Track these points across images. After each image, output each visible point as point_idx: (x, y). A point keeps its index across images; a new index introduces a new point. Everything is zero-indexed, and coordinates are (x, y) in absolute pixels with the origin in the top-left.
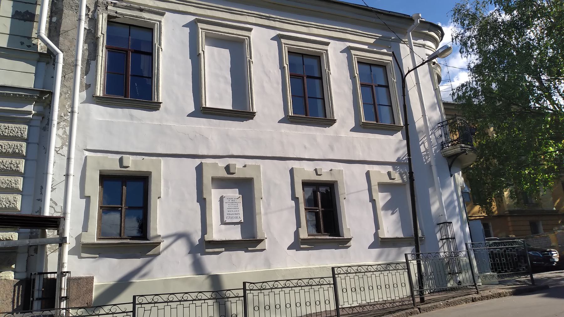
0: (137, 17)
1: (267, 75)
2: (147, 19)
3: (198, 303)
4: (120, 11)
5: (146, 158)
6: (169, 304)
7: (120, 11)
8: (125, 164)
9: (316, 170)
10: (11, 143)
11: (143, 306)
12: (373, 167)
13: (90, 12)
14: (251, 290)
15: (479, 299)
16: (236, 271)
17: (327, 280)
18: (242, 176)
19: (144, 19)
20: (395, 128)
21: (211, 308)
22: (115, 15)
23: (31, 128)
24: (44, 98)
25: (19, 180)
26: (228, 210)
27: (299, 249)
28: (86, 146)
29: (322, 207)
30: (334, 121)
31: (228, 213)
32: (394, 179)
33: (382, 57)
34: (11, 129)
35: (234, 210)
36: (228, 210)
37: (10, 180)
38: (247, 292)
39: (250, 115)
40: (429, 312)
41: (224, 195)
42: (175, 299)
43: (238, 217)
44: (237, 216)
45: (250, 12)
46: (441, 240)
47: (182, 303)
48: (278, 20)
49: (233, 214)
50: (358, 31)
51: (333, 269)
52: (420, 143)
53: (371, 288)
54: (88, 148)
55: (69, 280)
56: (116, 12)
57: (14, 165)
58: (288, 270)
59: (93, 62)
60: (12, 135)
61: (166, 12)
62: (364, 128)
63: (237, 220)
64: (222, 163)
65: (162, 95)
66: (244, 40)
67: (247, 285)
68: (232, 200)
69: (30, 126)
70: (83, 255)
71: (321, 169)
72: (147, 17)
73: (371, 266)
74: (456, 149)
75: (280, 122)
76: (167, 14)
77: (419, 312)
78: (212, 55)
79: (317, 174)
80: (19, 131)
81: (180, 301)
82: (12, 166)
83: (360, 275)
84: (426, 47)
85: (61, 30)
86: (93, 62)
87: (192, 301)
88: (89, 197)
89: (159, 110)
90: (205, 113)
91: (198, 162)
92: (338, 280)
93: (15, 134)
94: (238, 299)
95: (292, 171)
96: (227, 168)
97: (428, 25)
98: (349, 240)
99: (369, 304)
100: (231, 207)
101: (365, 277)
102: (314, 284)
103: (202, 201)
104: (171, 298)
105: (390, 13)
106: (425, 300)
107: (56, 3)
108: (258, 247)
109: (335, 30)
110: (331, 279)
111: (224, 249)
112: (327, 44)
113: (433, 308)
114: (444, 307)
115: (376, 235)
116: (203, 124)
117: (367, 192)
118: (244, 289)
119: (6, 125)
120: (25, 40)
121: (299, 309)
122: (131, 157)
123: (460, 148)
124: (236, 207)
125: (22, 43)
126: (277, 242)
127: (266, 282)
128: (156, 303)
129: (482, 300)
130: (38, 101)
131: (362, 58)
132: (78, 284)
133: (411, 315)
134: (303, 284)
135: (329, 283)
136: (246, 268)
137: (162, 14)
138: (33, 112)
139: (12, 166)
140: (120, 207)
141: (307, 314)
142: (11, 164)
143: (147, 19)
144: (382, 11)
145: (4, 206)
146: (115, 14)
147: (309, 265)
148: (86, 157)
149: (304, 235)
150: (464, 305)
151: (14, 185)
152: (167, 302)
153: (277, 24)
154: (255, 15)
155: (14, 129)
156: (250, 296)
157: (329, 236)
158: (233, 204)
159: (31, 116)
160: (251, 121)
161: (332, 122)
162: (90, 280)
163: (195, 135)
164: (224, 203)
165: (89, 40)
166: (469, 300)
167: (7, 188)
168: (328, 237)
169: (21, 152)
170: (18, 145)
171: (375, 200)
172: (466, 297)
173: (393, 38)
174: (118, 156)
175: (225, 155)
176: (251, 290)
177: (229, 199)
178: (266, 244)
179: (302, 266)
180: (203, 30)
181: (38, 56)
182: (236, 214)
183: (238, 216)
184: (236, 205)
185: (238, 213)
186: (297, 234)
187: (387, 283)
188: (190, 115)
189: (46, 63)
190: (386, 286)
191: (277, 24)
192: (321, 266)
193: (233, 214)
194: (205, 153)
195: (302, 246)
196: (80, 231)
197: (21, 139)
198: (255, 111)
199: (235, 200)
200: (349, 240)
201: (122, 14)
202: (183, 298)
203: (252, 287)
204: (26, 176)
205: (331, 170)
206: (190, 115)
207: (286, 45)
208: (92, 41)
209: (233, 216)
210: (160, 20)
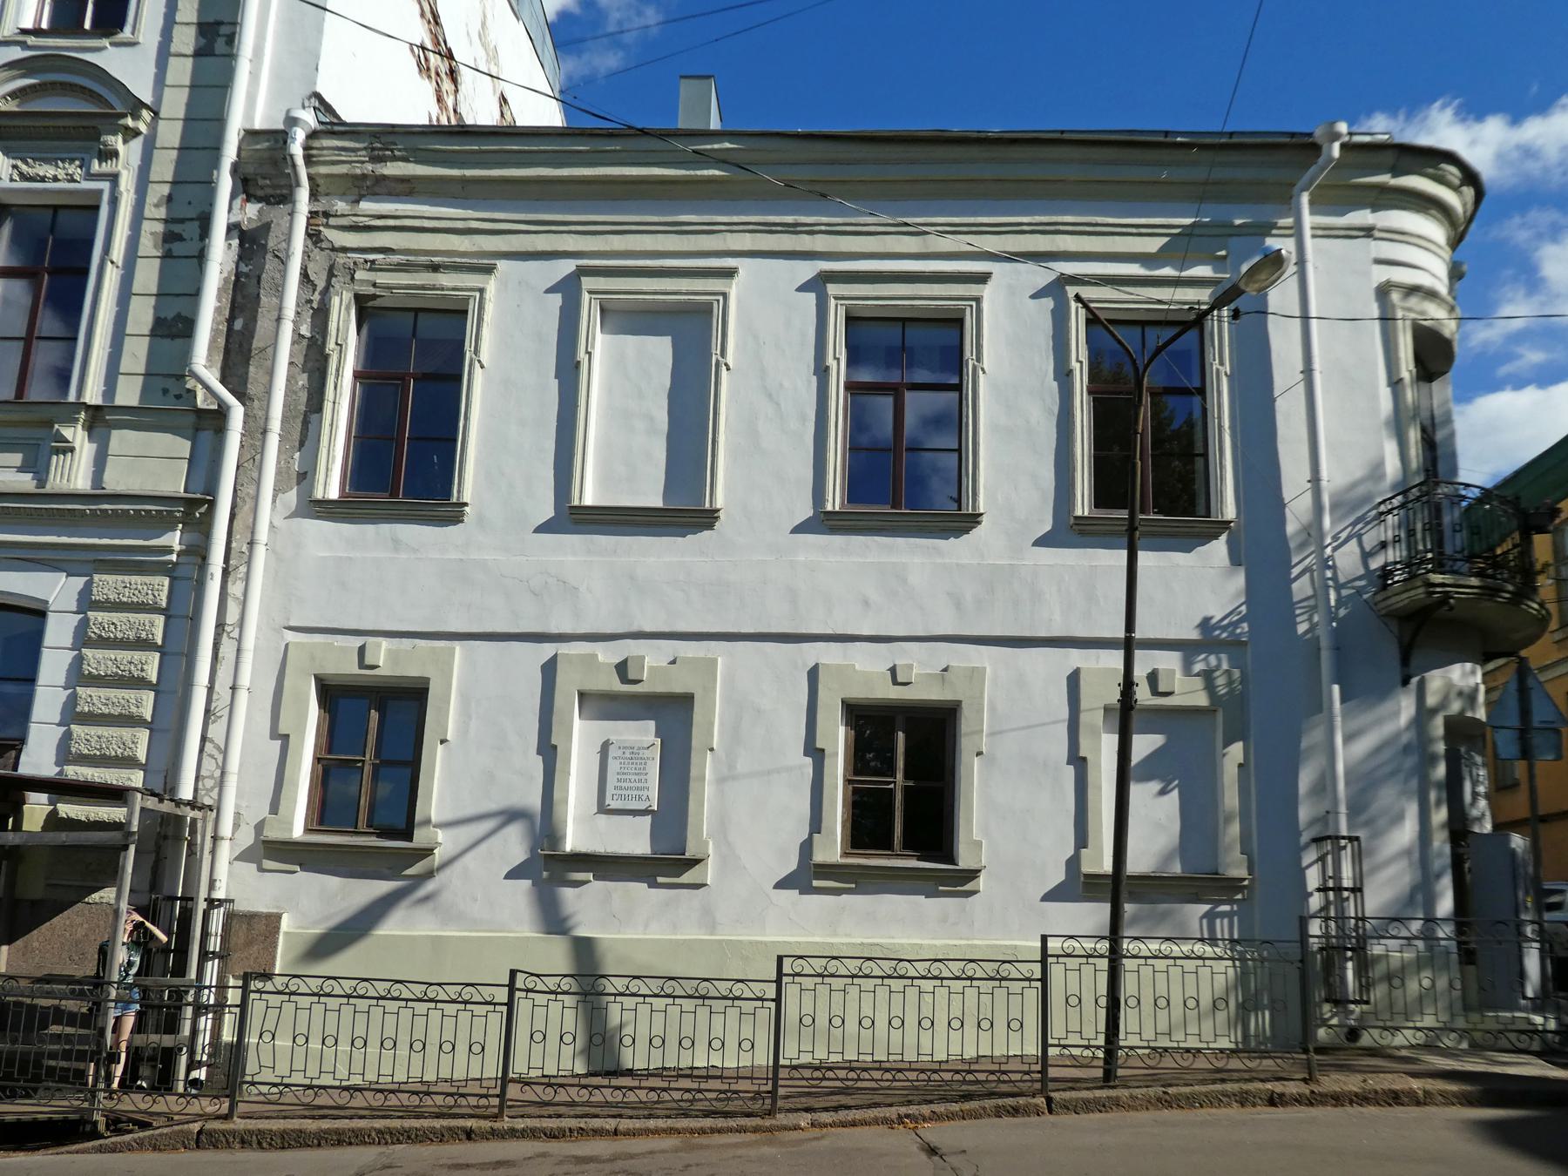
0: (423, 287)
1: (770, 396)
2: (448, 289)
3: (392, 1006)
4: (383, 278)
5: (417, 642)
6: (323, 999)
7: (383, 278)
8: (369, 661)
9: (893, 670)
10: (132, 617)
11: (264, 996)
12: (1098, 657)
13: (317, 293)
14: (528, 990)
15: (1296, 1100)
16: (619, 932)
18: (660, 688)
19: (443, 289)
20: (1197, 530)
21: (570, 1015)
22: (371, 290)
23: (176, 582)
24: (198, 515)
25: (144, 697)
26: (619, 777)
27: (807, 890)
28: (289, 620)
29: (907, 776)
30: (974, 520)
31: (619, 784)
33: (1185, 295)
34: (135, 586)
35: (633, 777)
36: (619, 777)
37: (127, 697)
38: (518, 994)
39: (705, 519)
40: (1083, 1116)
41: (613, 738)
42: (338, 991)
43: (644, 798)
44: (641, 793)
45: (735, 219)
46: (1319, 890)
47: (352, 1001)
48: (823, 228)
49: (631, 788)
50: (1100, 220)
52: (1295, 572)
54: (293, 623)
55: (230, 917)
56: (374, 285)
57: (136, 665)
58: (761, 942)
59: (314, 417)
60: (135, 600)
61: (497, 262)
62: (1082, 533)
63: (642, 806)
64: (607, 654)
65: (470, 483)
66: (710, 304)
67: (520, 977)
68: (633, 752)
69: (173, 579)
70: (268, 864)
71: (910, 667)
72: (450, 284)
73: (909, 961)
74: (1412, 593)
75: (800, 529)
76: (502, 265)
77: (1046, 1111)
78: (617, 363)
79: (895, 682)
80: (150, 592)
81: (349, 996)
82: (132, 668)
84: (1377, 234)
85: (254, 346)
86: (314, 417)
87: (378, 999)
88: (288, 736)
89: (462, 521)
90: (577, 522)
91: (547, 650)
93: (142, 599)
94: (491, 1008)
95: (813, 674)
96: (622, 668)
97: (1389, 157)
98: (972, 874)
99: (879, 1066)
100: (626, 771)
102: (713, 993)
103: (549, 751)
104: (833, 966)
105: (1235, 140)
107: (244, 283)
108: (686, 878)
111: (590, 876)
112: (983, 278)
113: (1104, 1106)
114: (1147, 1109)
115: (1073, 863)
116: (573, 548)
117: (1063, 730)
118: (511, 987)
119: (127, 578)
120: (170, 384)
121: (926, 1038)
122: (385, 643)
123: (1421, 590)
124: (640, 769)
125: (165, 391)
126: (745, 868)
127: (334, 978)
128: (798, 975)
129: (1312, 1104)
130: (188, 522)
132: (250, 928)
133: (1014, 1116)
135: (760, 995)
136: (646, 926)
137: (489, 270)
138: (177, 547)
139: (132, 668)
140: (359, 761)
141: (455, 1077)
142: (130, 663)
143: (448, 289)
144: (1259, 140)
145: (113, 754)
146: (371, 288)
147: (835, 934)
148: (287, 645)
150: (1234, 1112)
151: (134, 709)
152: (320, 996)
153: (820, 243)
154: (751, 227)
155: (139, 587)
156: (523, 1006)
157: (918, 860)
158: (632, 763)
159: (174, 557)
160: (707, 533)
161: (965, 522)
162: (273, 921)
163: (546, 583)
164: (610, 760)
165: (310, 365)
166: (1254, 1097)
167: (121, 715)
168: (913, 863)
169: (150, 636)
170: (147, 623)
171: (1084, 759)
172: (1246, 1087)
173: (1238, 222)
174: (357, 642)
175: (620, 631)
176: (528, 990)
177: (624, 748)
178: (710, 872)
179: (813, 935)
180: (593, 296)
181: (191, 418)
182: (638, 789)
183: (645, 793)
184: (641, 764)
185: (645, 785)
186: (806, 848)
188: (543, 529)
189: (211, 432)
190: (840, 1023)
191: (820, 243)
192: (865, 941)
193: (631, 788)
194: (567, 628)
195: (816, 883)
196: (264, 811)
197: (153, 609)
198: (718, 506)
199: (641, 752)
200: (972, 874)
201: (389, 288)
202: (355, 990)
203: (799, 966)
204: (161, 688)
205: (945, 670)
206: (543, 529)
207: (843, 302)
208: (317, 365)
209: (629, 792)
210: (481, 286)
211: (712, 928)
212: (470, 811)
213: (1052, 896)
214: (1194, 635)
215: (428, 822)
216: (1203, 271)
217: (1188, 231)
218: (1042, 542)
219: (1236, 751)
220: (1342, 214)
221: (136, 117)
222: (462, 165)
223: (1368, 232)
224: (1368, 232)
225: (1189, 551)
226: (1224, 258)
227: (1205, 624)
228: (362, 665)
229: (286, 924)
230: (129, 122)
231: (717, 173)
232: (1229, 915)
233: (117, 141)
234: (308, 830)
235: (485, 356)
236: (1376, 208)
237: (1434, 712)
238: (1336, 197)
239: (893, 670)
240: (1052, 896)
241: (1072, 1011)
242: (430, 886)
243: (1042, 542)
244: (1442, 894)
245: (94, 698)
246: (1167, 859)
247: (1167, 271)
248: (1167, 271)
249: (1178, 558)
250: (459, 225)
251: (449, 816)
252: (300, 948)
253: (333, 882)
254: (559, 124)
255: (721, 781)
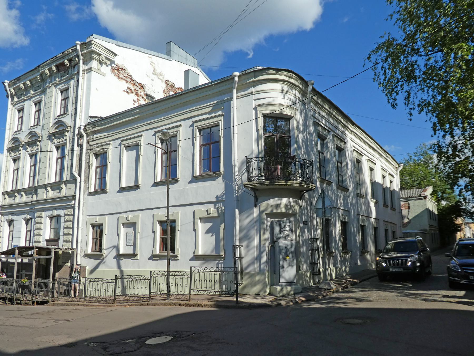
9: (207, 211)
17: (113, 280)
18: (132, 222)
32: (210, 214)
50: (170, 116)
51: (151, 272)
53: (138, 288)
64: (125, 215)
70: (86, 258)
75: (118, 192)
83: (95, 283)
92: (193, 274)
97: (252, 74)
101: (161, 278)
106: (377, 277)
109: (186, 113)
110: (114, 280)
112: (179, 126)
122: (98, 217)
131: (111, 126)
134: (175, 275)
149: (158, 252)
162: (85, 267)
187: (206, 278)
211: (139, 268)
212: (109, 247)
213: (191, 260)
214: (215, 200)
215: (103, 249)
216: (219, 113)
217: (216, 104)
218: (190, 182)
219: (223, 226)
220: (247, 90)
221: (68, 128)
222: (105, 125)
223: (251, 93)
224: (251, 93)
225: (215, 180)
226: (223, 108)
227: (217, 197)
228: (208, 214)
229: (87, 268)
230: (67, 130)
231: (138, 116)
232: (221, 263)
233: (66, 133)
234: (160, 252)
235: (142, 153)
236: (254, 86)
237: (263, 211)
238: (243, 87)
239: (207, 211)
240: (191, 260)
241: (163, 282)
242: (104, 261)
243: (190, 182)
244: (264, 256)
245: (70, 231)
246: (212, 251)
247: (213, 115)
248: (213, 115)
249: (213, 182)
250: (106, 136)
251: (107, 248)
252: (89, 272)
253: (93, 260)
254: (207, 81)
255: (141, 238)
